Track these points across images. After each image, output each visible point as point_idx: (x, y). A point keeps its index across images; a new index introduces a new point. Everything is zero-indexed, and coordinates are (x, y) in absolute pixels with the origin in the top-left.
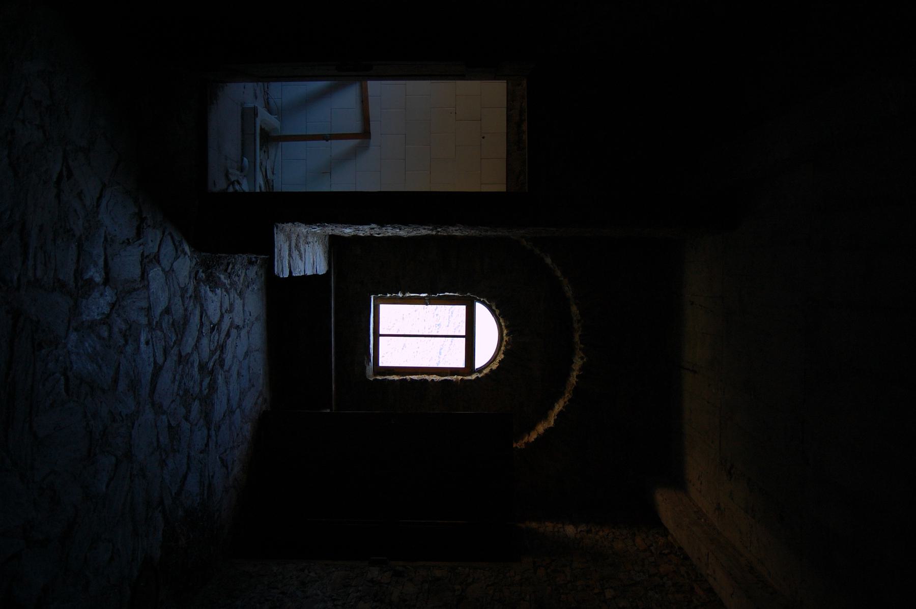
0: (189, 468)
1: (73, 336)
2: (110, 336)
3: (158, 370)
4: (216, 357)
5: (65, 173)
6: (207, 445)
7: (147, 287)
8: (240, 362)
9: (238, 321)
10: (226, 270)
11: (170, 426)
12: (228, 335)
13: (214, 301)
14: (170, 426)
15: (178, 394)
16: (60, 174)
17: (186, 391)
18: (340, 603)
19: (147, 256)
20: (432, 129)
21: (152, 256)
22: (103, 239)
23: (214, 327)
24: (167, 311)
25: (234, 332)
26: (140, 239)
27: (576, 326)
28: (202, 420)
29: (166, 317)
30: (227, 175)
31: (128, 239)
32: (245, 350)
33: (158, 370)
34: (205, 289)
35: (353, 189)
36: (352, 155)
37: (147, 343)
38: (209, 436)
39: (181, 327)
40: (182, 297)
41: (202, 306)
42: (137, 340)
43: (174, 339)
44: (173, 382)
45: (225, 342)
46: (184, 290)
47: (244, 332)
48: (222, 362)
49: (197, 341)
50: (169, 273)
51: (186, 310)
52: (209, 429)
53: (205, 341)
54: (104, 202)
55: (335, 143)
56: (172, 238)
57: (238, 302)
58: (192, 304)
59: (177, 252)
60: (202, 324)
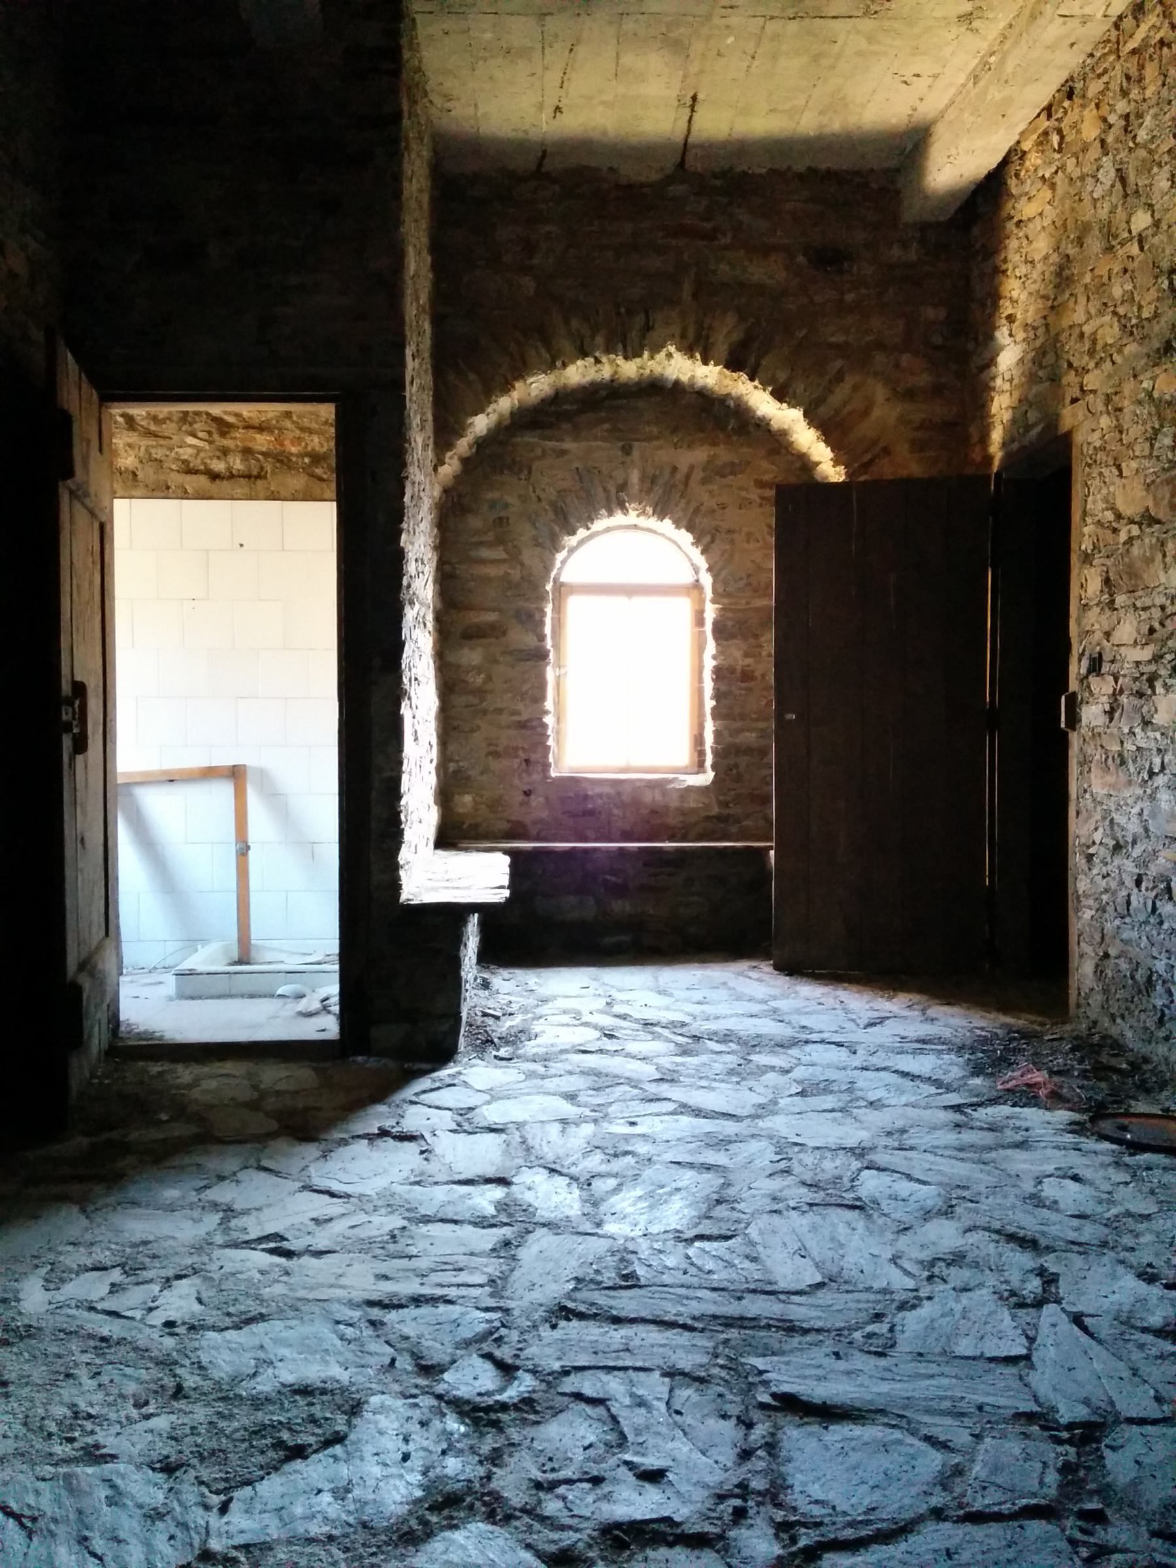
0: (884, 1069)
1: (610, 1228)
2: (616, 1175)
3: (684, 1109)
4: (666, 1032)
5: (272, 1245)
6: (839, 1045)
7: (520, 1126)
8: (677, 1001)
9: (601, 1003)
10: (497, 1018)
11: (802, 1094)
12: (624, 1017)
13: (552, 1033)
14: (802, 1094)
15: (738, 1083)
16: (272, 1251)
17: (731, 1072)
18: (1157, 761)
19: (459, 1125)
20: (209, 624)
21: (459, 1118)
22: (417, 1187)
23: (606, 1035)
24: (571, 1097)
25: (618, 1009)
26: (422, 1136)
27: (606, 372)
28: (790, 1052)
29: (582, 1098)
30: (310, 1015)
31: (422, 1152)
32: (654, 995)
33: (684, 1109)
34: (530, 1048)
35: (337, 797)
36: (275, 798)
37: (633, 1124)
38: (822, 1042)
39: (602, 1081)
40: (543, 1077)
41: (562, 1052)
42: (626, 1138)
43: (628, 1088)
44: (713, 1089)
45: (637, 1021)
46: (530, 1075)
47: (619, 996)
48: (672, 1025)
49: (634, 1057)
50: (494, 1095)
51: (570, 1073)
52: (807, 1042)
53: (633, 1047)
54: (336, 1187)
55: (253, 837)
56: (424, 1092)
57: (561, 1003)
58: (558, 1065)
59: (454, 1085)
60: (601, 1051)
